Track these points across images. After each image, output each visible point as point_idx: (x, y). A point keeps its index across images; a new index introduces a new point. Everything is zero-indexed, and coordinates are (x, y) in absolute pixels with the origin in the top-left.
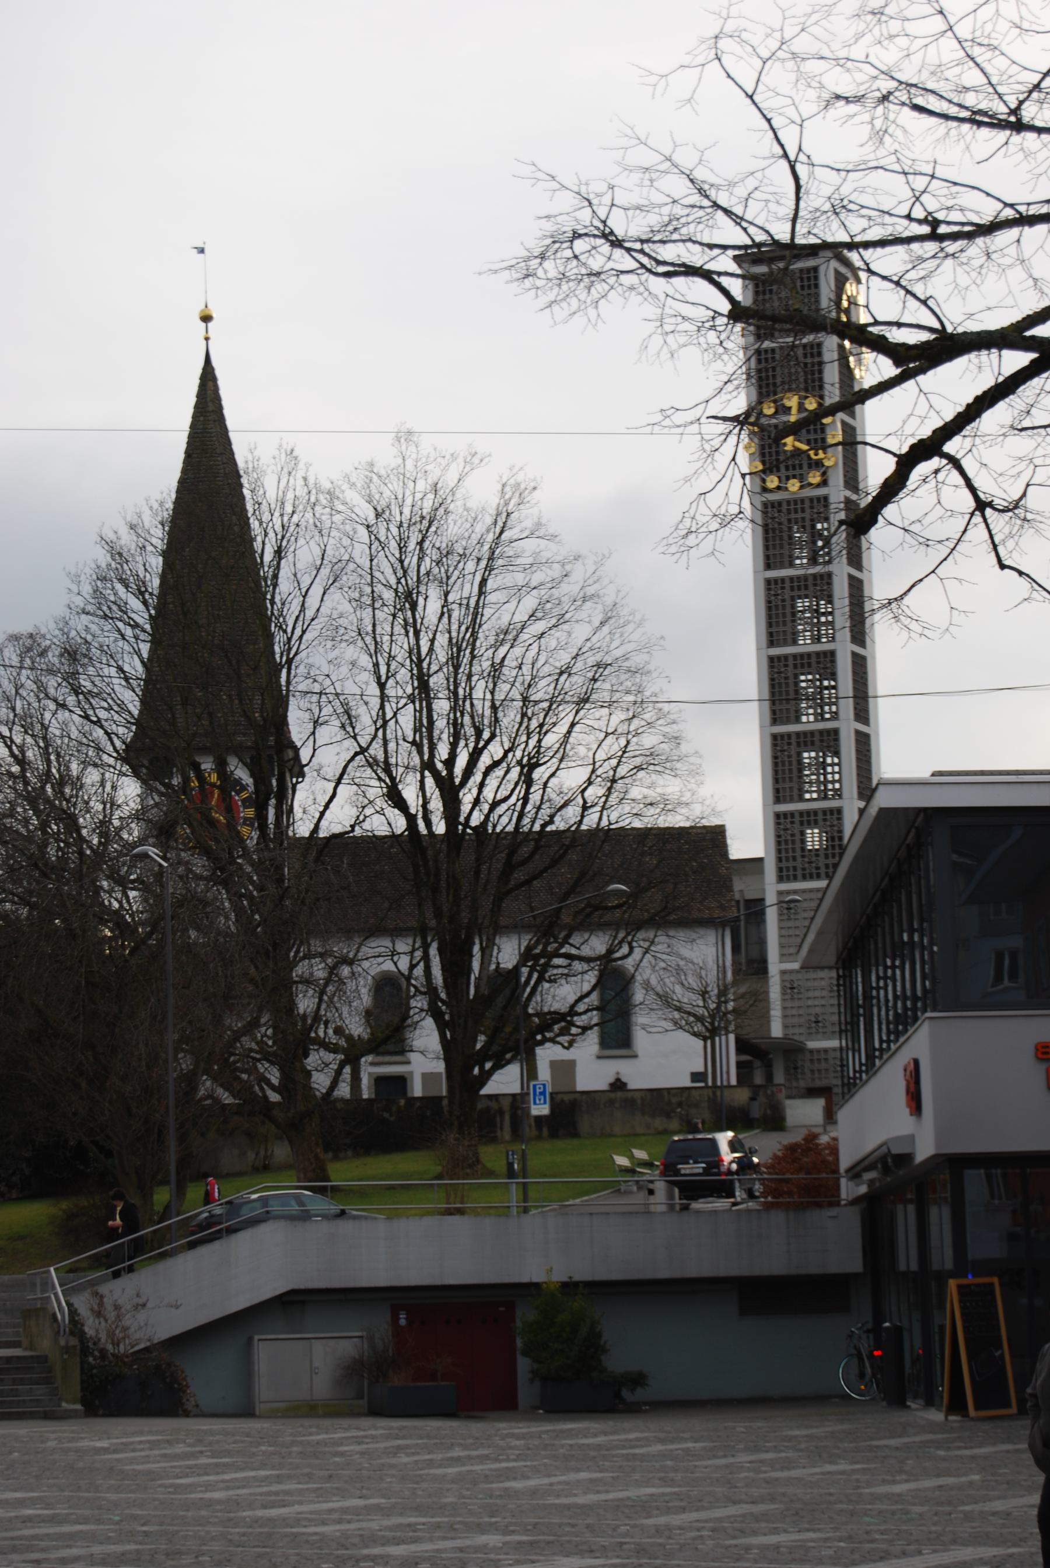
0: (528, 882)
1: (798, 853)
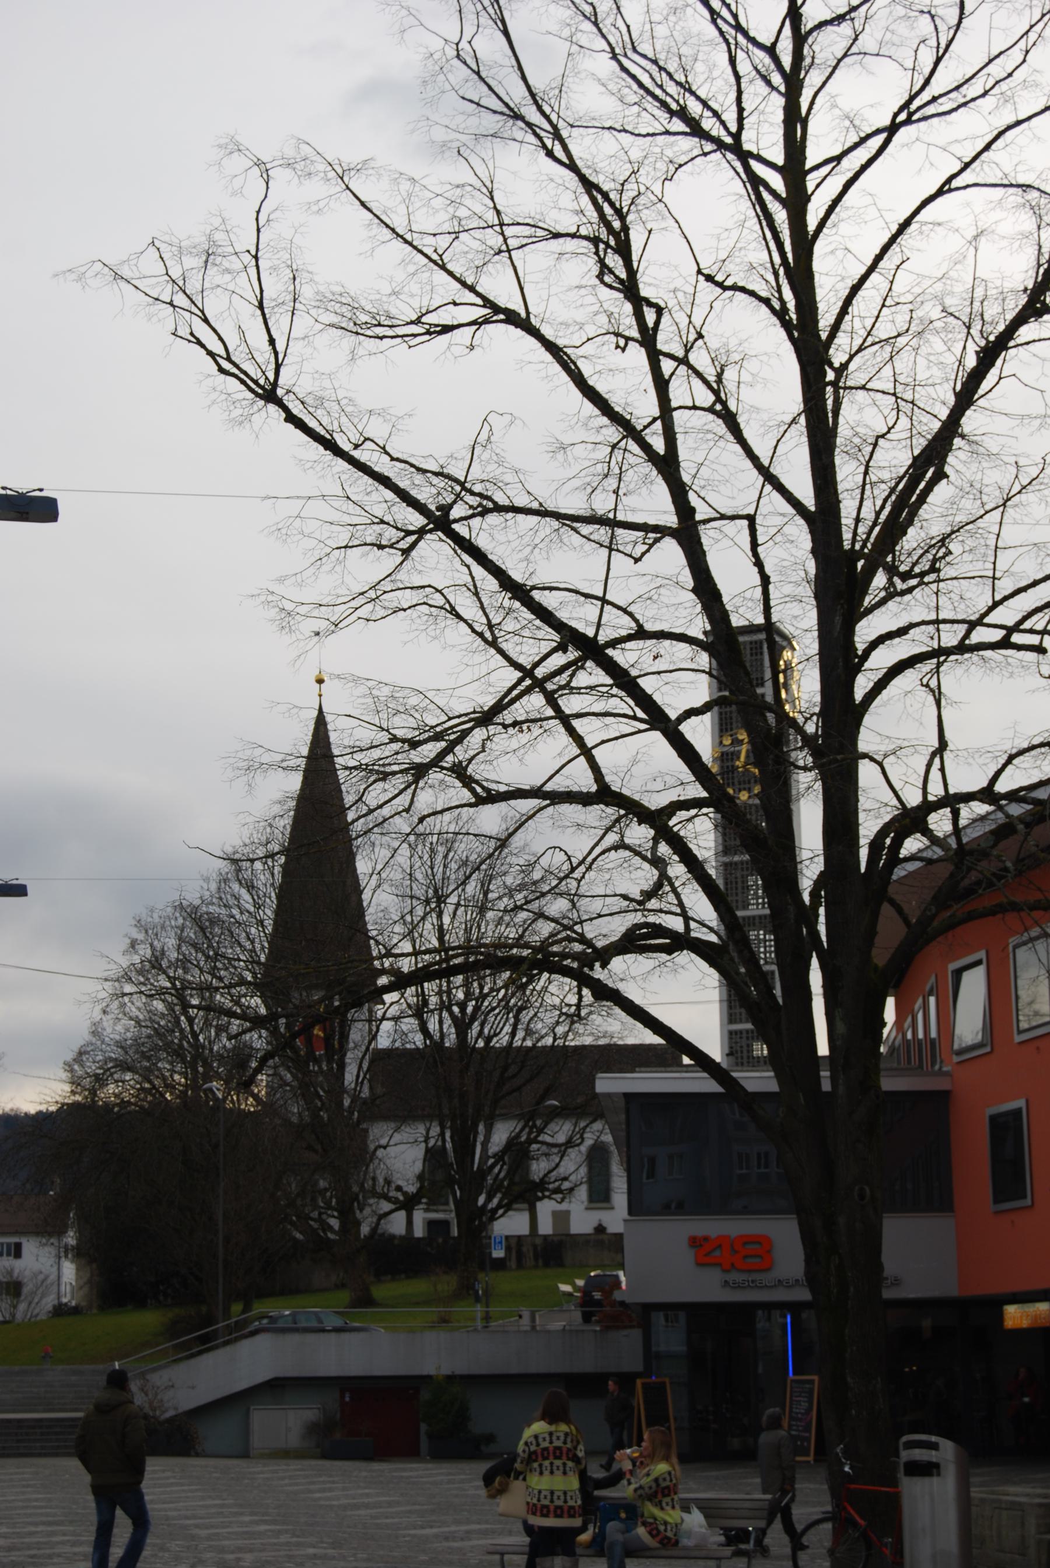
0: (519, 1089)
1: (745, 1060)
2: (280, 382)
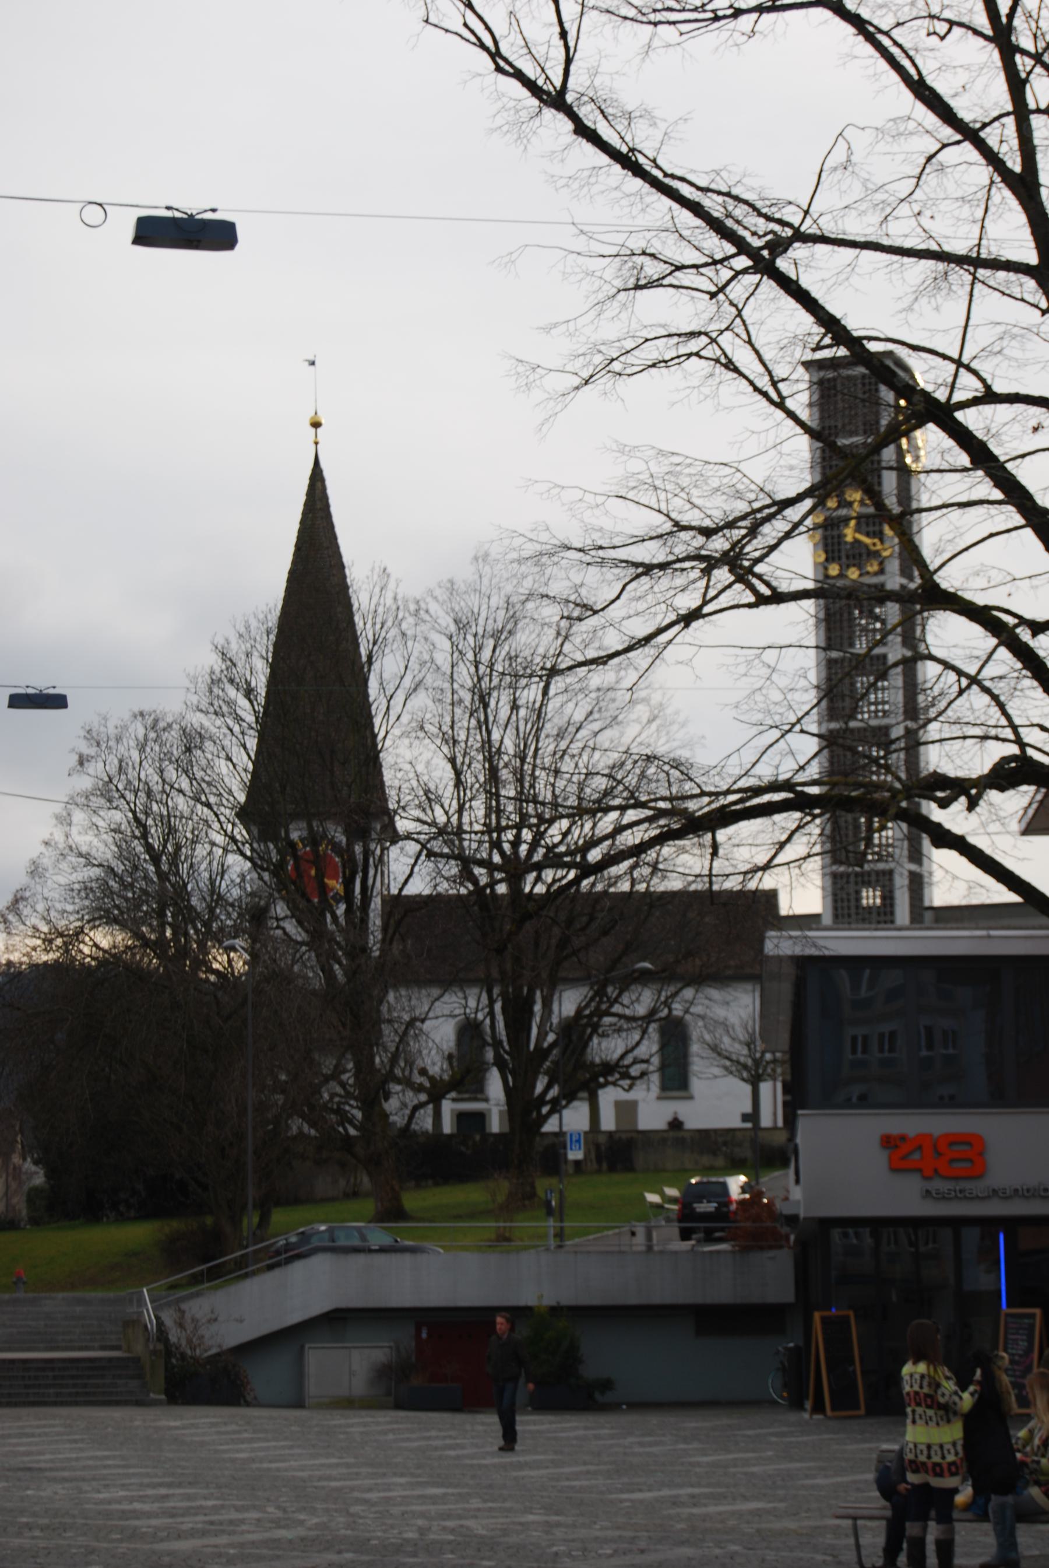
1: (853, 911)
2: (571, 84)
